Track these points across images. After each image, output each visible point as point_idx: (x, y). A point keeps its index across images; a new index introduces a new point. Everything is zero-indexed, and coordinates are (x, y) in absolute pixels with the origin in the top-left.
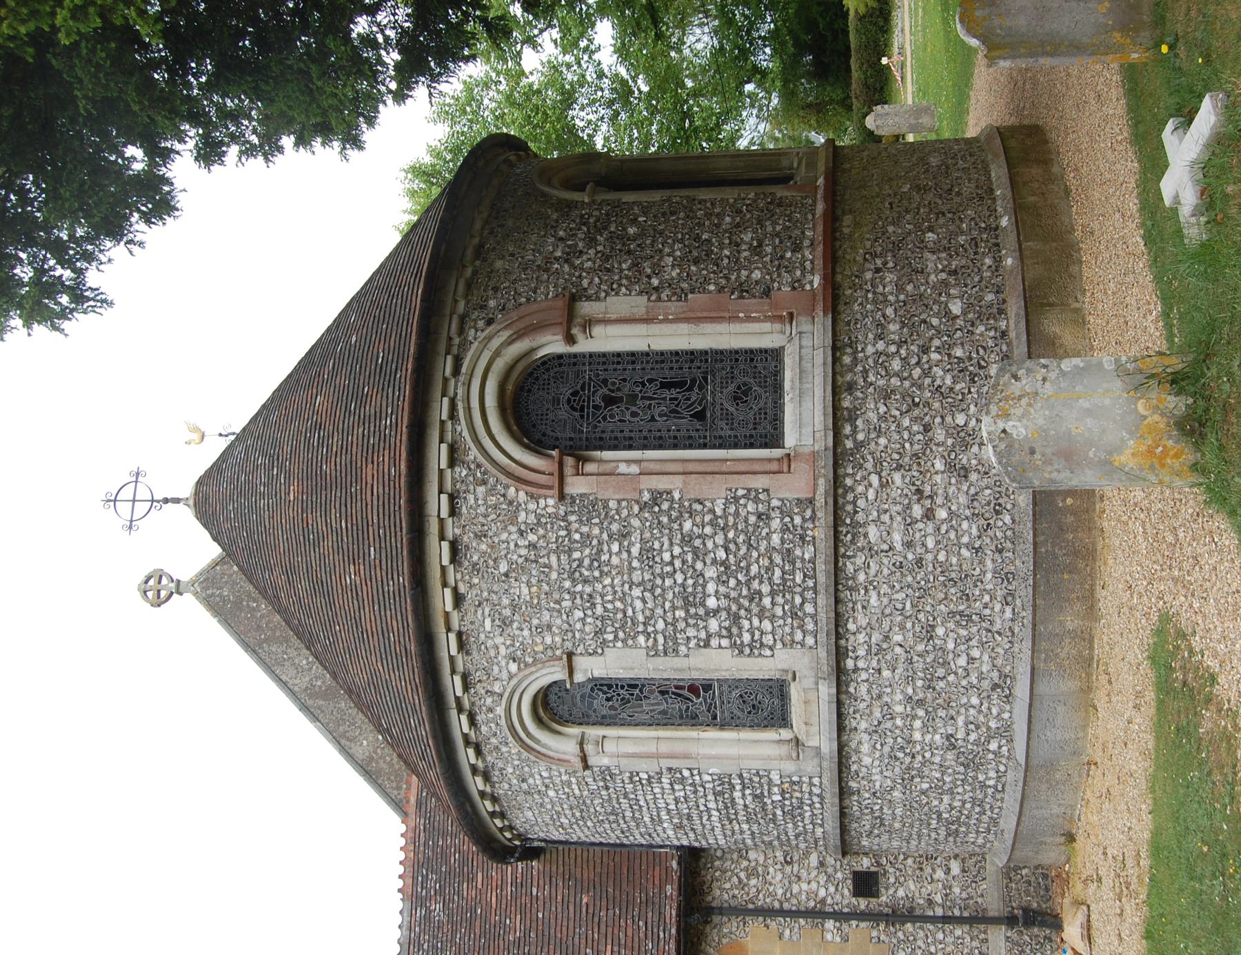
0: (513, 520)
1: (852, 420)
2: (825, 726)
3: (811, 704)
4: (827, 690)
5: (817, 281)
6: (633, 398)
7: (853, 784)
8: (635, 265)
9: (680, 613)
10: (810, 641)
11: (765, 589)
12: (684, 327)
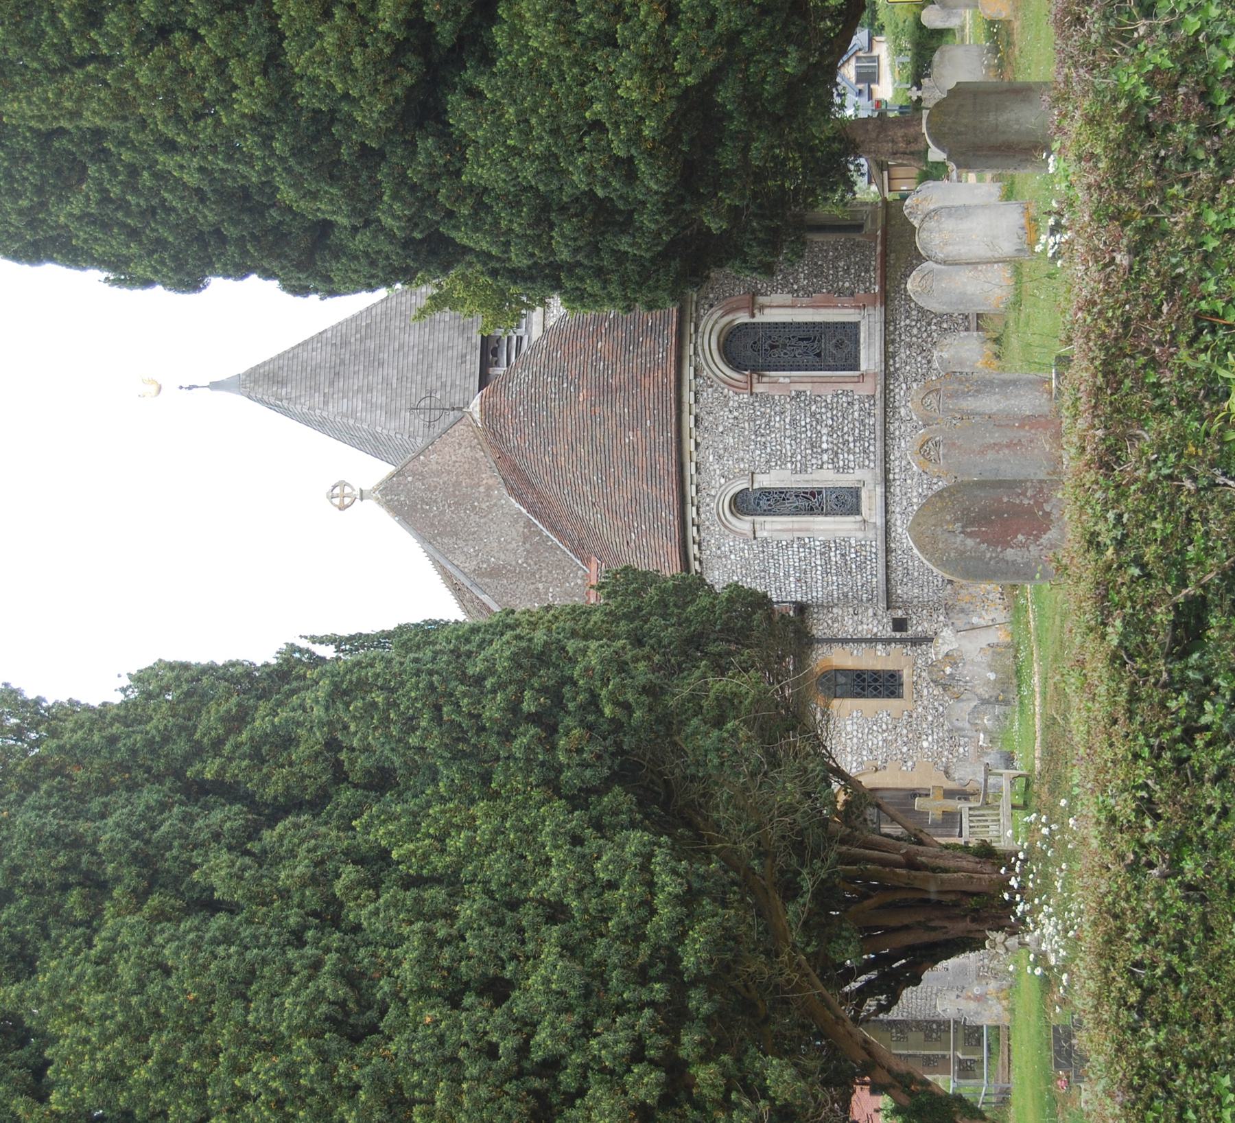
0: (726, 405)
1: (894, 358)
2: (879, 510)
3: (871, 501)
4: (880, 490)
5: (877, 289)
6: (784, 346)
7: (892, 545)
8: (784, 277)
9: (809, 451)
10: (872, 465)
11: (851, 439)
12: (811, 311)
